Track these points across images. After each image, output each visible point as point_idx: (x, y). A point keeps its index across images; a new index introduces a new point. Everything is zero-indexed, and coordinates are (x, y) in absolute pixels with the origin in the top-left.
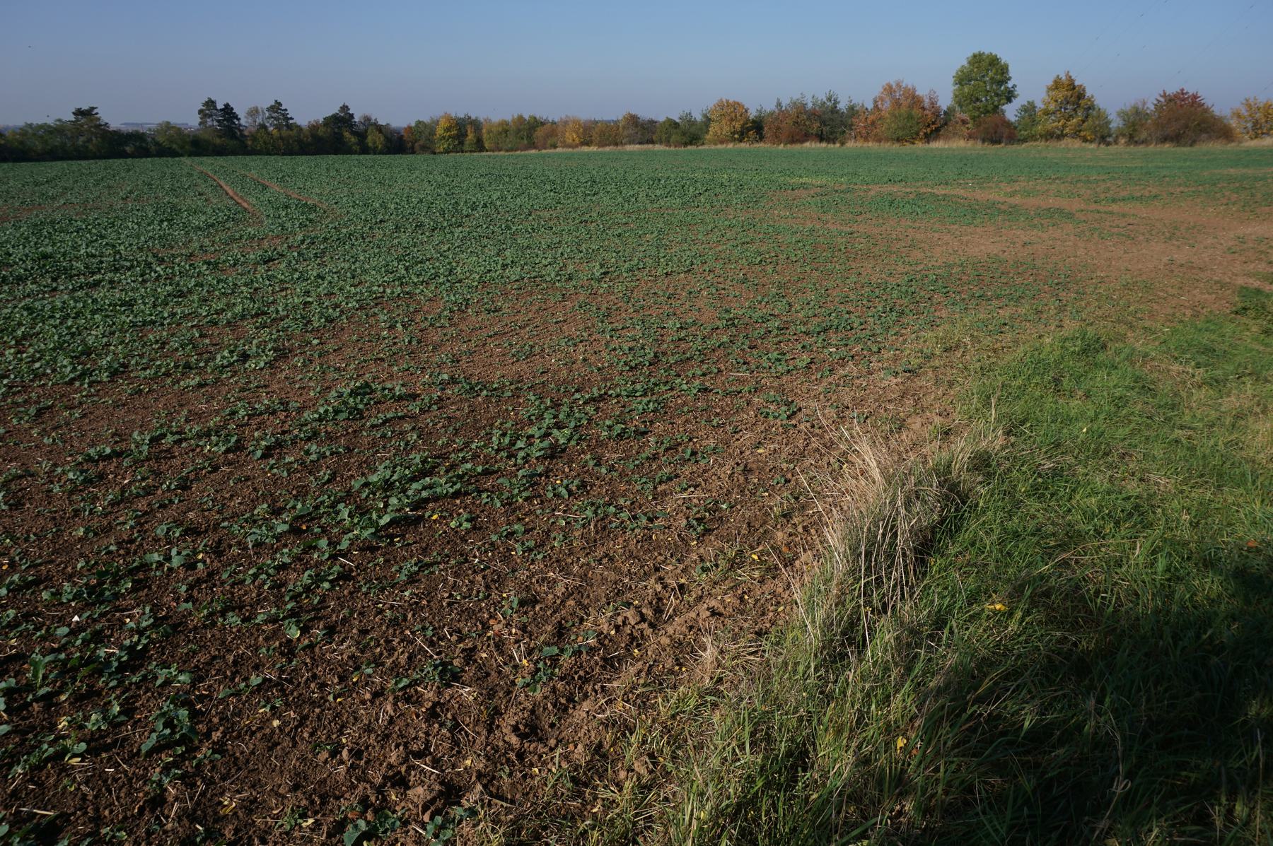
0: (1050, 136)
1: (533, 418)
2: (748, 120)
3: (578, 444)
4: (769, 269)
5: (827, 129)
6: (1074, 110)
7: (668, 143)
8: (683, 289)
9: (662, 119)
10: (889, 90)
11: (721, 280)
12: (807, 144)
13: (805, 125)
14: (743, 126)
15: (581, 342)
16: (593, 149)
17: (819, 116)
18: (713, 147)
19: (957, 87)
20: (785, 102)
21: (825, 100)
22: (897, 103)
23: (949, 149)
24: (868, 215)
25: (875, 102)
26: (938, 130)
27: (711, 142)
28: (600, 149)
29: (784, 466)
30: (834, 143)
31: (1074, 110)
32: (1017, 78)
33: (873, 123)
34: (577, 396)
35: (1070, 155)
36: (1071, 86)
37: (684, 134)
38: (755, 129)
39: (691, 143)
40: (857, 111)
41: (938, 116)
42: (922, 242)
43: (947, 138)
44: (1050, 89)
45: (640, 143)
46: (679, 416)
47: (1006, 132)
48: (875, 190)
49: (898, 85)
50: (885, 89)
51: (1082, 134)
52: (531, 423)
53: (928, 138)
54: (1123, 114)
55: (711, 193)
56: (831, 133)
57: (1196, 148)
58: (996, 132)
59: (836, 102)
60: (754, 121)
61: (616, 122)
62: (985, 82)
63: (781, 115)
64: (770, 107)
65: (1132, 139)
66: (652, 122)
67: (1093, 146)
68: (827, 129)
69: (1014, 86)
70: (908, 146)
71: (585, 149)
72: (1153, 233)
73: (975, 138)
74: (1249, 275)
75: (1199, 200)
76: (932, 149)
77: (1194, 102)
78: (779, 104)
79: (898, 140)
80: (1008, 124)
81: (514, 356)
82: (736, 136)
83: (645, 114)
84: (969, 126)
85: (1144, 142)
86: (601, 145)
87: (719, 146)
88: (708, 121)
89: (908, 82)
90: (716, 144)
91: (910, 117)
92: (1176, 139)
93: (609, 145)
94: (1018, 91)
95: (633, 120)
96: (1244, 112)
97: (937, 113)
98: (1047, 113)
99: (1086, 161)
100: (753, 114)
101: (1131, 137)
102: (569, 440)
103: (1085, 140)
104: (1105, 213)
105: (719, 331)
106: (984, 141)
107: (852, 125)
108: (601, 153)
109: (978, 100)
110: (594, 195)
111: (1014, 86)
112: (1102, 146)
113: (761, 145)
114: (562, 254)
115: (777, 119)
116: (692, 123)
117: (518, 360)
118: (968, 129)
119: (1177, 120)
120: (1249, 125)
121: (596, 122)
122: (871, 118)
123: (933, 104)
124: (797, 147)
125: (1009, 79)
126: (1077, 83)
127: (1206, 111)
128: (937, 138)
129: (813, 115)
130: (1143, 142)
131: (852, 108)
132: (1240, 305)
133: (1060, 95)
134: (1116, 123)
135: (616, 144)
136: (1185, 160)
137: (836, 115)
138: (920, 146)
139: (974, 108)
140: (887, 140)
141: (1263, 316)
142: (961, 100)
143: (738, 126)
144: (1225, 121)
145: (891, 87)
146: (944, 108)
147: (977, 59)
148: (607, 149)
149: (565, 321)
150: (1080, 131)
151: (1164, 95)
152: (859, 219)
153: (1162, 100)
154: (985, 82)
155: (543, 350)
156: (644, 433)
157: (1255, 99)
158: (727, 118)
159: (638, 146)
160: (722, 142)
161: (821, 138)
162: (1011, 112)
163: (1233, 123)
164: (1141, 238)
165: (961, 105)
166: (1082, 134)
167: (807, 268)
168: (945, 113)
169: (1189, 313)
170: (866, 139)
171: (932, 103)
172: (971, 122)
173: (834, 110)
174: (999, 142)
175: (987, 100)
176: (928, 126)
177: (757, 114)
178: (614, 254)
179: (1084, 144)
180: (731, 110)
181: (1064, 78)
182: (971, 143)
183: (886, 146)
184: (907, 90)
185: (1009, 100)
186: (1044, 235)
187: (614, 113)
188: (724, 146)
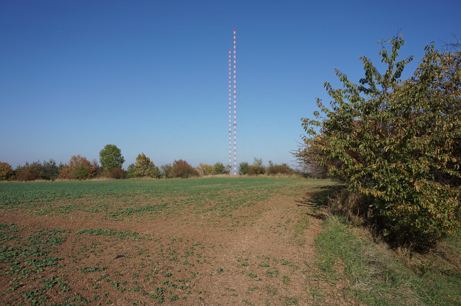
0: (139, 175)
6: (147, 166)
12: (37, 181)
13: (36, 172)
19: (101, 157)
20: (30, 163)
21: (49, 162)
23: (99, 181)
30: (49, 180)
36: (145, 158)
44: (137, 159)
47: (122, 174)
49: (79, 156)
50: (73, 158)
57: (189, 179)
58: (118, 174)
59: (54, 163)
65: (167, 176)
76: (92, 181)
79: (78, 178)
85: (171, 177)
89: (83, 155)
92: (181, 175)
96: (200, 167)
101: (167, 175)
103: (152, 177)
106: (114, 178)
111: (123, 157)
120: (203, 172)
124: (32, 182)
126: (146, 157)
127: (189, 166)
130: (171, 177)
133: (141, 161)
134: (162, 171)
136: (185, 183)
137: (54, 169)
140: (73, 178)
144: (196, 170)
145: (75, 157)
147: (109, 147)
151: (176, 161)
153: (175, 163)
157: (203, 163)
161: (44, 178)
163: (198, 170)
174: (120, 178)
183: (73, 181)
184: (82, 159)
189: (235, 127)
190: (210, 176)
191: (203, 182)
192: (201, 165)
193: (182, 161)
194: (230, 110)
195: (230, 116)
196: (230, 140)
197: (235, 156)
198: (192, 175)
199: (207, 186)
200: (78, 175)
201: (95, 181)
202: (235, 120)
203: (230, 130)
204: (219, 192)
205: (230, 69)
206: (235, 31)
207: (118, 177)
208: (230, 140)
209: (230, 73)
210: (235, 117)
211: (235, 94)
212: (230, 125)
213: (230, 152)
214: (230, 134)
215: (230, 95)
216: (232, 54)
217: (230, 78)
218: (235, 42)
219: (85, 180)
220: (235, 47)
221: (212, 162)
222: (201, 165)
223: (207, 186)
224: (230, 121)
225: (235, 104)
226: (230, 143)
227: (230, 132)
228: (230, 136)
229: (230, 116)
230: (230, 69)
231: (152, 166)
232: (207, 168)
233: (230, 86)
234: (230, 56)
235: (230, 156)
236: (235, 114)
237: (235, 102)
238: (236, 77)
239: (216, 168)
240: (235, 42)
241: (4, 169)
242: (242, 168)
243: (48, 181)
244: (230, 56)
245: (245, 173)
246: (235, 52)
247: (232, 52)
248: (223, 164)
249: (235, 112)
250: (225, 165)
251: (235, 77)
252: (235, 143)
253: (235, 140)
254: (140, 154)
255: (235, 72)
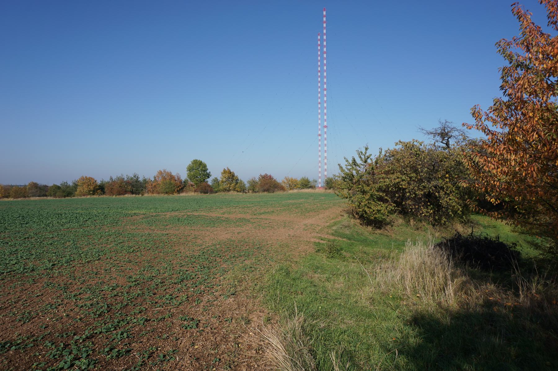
0: (225, 190)
1: (57, 357)
2: (96, 185)
3: (95, 367)
4: (139, 254)
5: (134, 189)
6: (232, 181)
7: (55, 196)
8: (101, 269)
9: (50, 184)
10: (160, 173)
11: (118, 262)
12: (126, 195)
14: (94, 188)
15: (59, 305)
16: (11, 199)
17: (131, 184)
18: (80, 197)
21: (132, 177)
22: (164, 178)
23: (188, 196)
24: (171, 226)
25: (155, 178)
26: (182, 189)
27: (78, 195)
28: (15, 200)
29: (213, 352)
31: (232, 181)
32: (210, 169)
33: (155, 186)
34: (76, 337)
35: (234, 197)
37: (64, 192)
38: (101, 189)
39: (68, 196)
40: (147, 182)
41: (182, 183)
42: (199, 236)
43: (187, 192)
44: (222, 173)
45: (39, 196)
46: (142, 337)
48: (168, 215)
49: (165, 171)
50: (159, 173)
51: (236, 189)
52: (56, 360)
53: (179, 192)
54: (249, 182)
55: (92, 219)
56: (137, 190)
57: (275, 193)
58: (205, 189)
60: (99, 186)
61: (25, 186)
62: (199, 171)
63: (113, 183)
64: (107, 179)
65: (254, 191)
66: (46, 186)
67: (241, 194)
68: (134, 189)
69: (210, 172)
70: (171, 195)
71: (6, 199)
72: (279, 225)
73: (197, 192)
74: (315, 237)
75: (287, 212)
76: (181, 196)
77: (270, 178)
78: (111, 178)
79: (166, 193)
80: (209, 186)
81: (20, 320)
82: (91, 192)
83: (41, 182)
84: (195, 187)
86: (15, 197)
87: (83, 197)
88: (76, 186)
89: (168, 170)
90: (81, 196)
91: (171, 184)
92: (267, 190)
93: (20, 197)
94: (211, 173)
95: (35, 186)
96: (285, 181)
97: (181, 182)
98: (223, 182)
99: (240, 199)
100: (99, 182)
101: (253, 190)
102: (88, 366)
103: (238, 192)
104: (260, 219)
105: (132, 288)
106: (201, 193)
107: (145, 187)
108: (16, 202)
109: (197, 177)
110: (27, 224)
111: (210, 172)
112: (244, 194)
113: (104, 196)
114: (21, 257)
115: (111, 185)
116: (68, 187)
117: (24, 323)
118: (194, 188)
119: (267, 184)
120: (288, 185)
121: (12, 186)
122: (154, 184)
123: (179, 178)
124: (122, 196)
125: (207, 169)
127: (275, 180)
128: (182, 192)
129: (128, 183)
131: (145, 180)
132: (317, 249)
133: (227, 176)
134: (247, 185)
135: (25, 197)
138: (176, 195)
139: (196, 180)
140: (162, 193)
141: (325, 252)
142: (191, 177)
143: (92, 188)
145: (161, 172)
146: (183, 180)
148: (19, 199)
149: (42, 295)
150: (235, 188)
151: (261, 176)
152: (168, 227)
154: (199, 171)
155: (38, 314)
156: (128, 352)
158: (86, 184)
159: (37, 198)
160: (84, 195)
161: (132, 193)
162: (210, 181)
163: (283, 185)
164: (276, 227)
165: (191, 179)
166: (236, 189)
167: (156, 252)
168: (184, 182)
169: (304, 253)
170: (153, 193)
171: (178, 178)
172: (195, 185)
173: (137, 181)
175: (200, 177)
176: (178, 187)
177: (101, 183)
178: (54, 255)
179: (238, 193)
180: (88, 181)
181: (227, 169)
182: (196, 193)
183: (162, 195)
185: (208, 177)
186: (243, 229)
187: (24, 181)
188: (85, 197)
189: (325, 130)
190: (295, 191)
191: (291, 197)
192: (286, 179)
193: (268, 175)
194: (319, 108)
195: (319, 116)
196: (320, 146)
197: (326, 164)
198: (278, 190)
199: (294, 201)
200: (167, 190)
201: (185, 196)
202: (325, 120)
203: (320, 132)
204: (301, 206)
205: (319, 58)
206: (325, 11)
207: (205, 192)
208: (320, 146)
209: (319, 64)
210: (325, 117)
211: (325, 90)
212: (320, 127)
213: (320, 159)
214: (320, 138)
215: (319, 90)
216: (322, 40)
217: (319, 69)
218: (325, 25)
219: (174, 195)
220: (325, 31)
221: (298, 176)
222: (286, 179)
223: (294, 201)
224: (320, 122)
225: (325, 102)
226: (320, 148)
227: (320, 135)
228: (320, 140)
229: (319, 116)
230: (319, 58)
231: (237, 180)
232: (292, 182)
233: (319, 79)
234: (319, 43)
235: (320, 165)
236: (325, 114)
237: (325, 99)
238: (327, 69)
239: (302, 183)
240: (325, 25)
241: (90, 184)
242: (327, 183)
243: (138, 196)
244: (319, 43)
245: (330, 188)
246: (325, 37)
247: (322, 37)
248: (309, 179)
249: (325, 111)
250: (311, 179)
251: (325, 68)
252: (326, 148)
253: (325, 145)
254: (224, 169)
255: (325, 62)
